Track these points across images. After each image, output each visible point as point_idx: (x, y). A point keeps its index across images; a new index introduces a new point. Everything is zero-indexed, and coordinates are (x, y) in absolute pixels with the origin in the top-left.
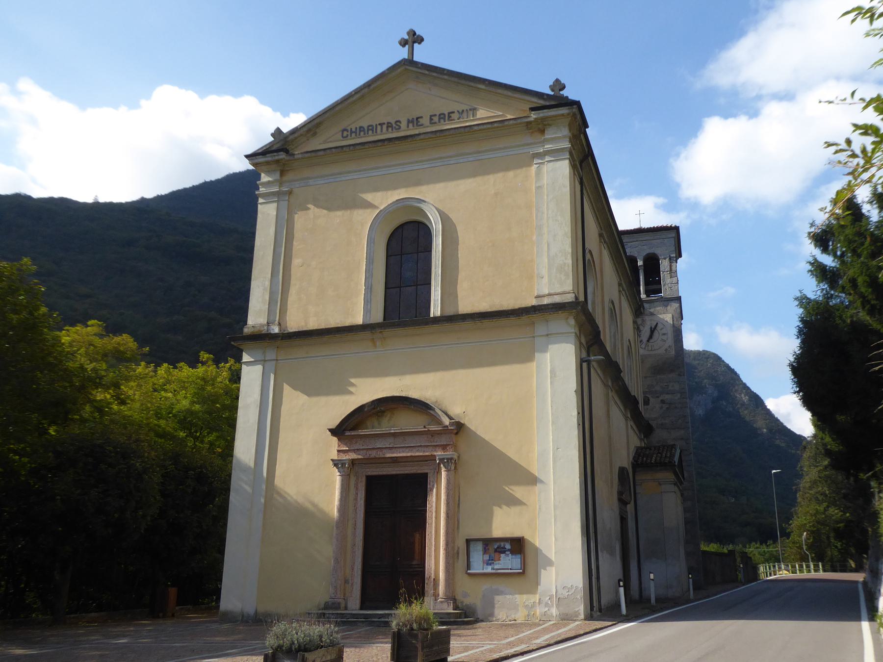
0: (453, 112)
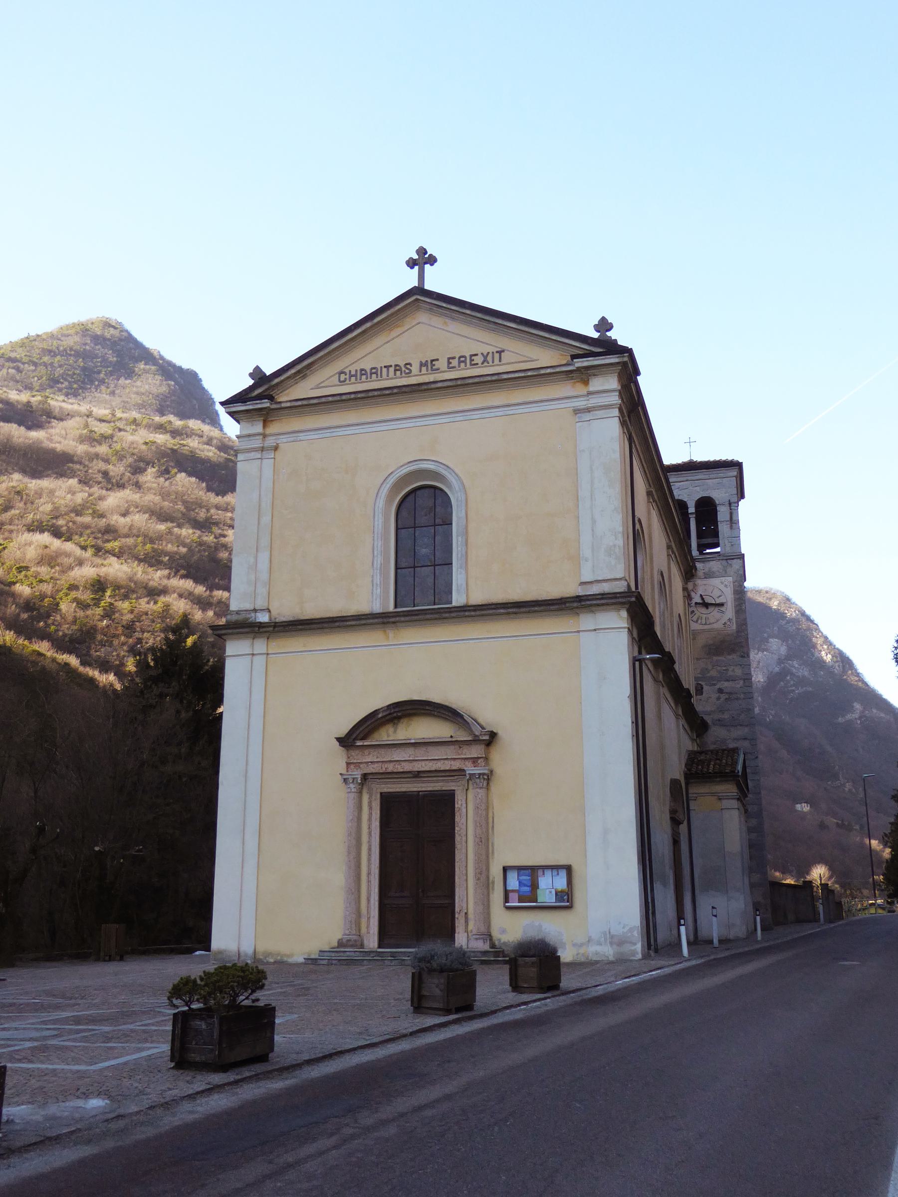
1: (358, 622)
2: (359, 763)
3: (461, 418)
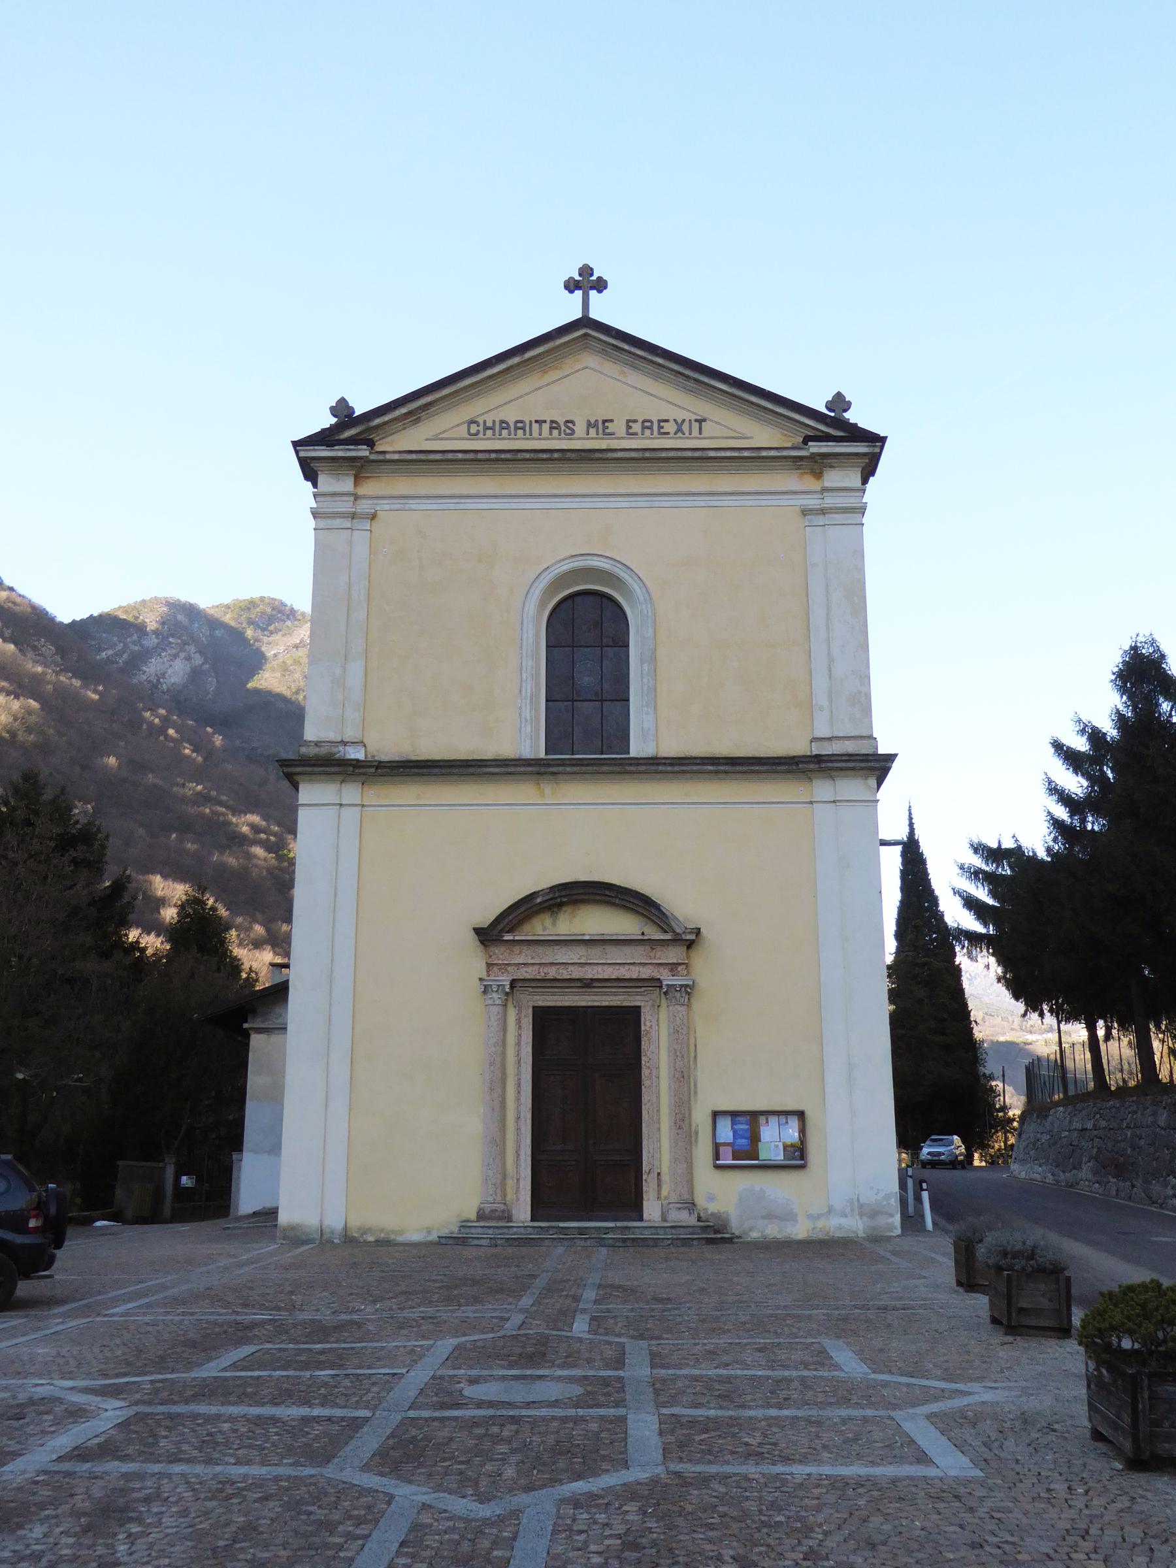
0: (667, 421)
1: (503, 770)
2: (507, 964)
3: (647, 504)
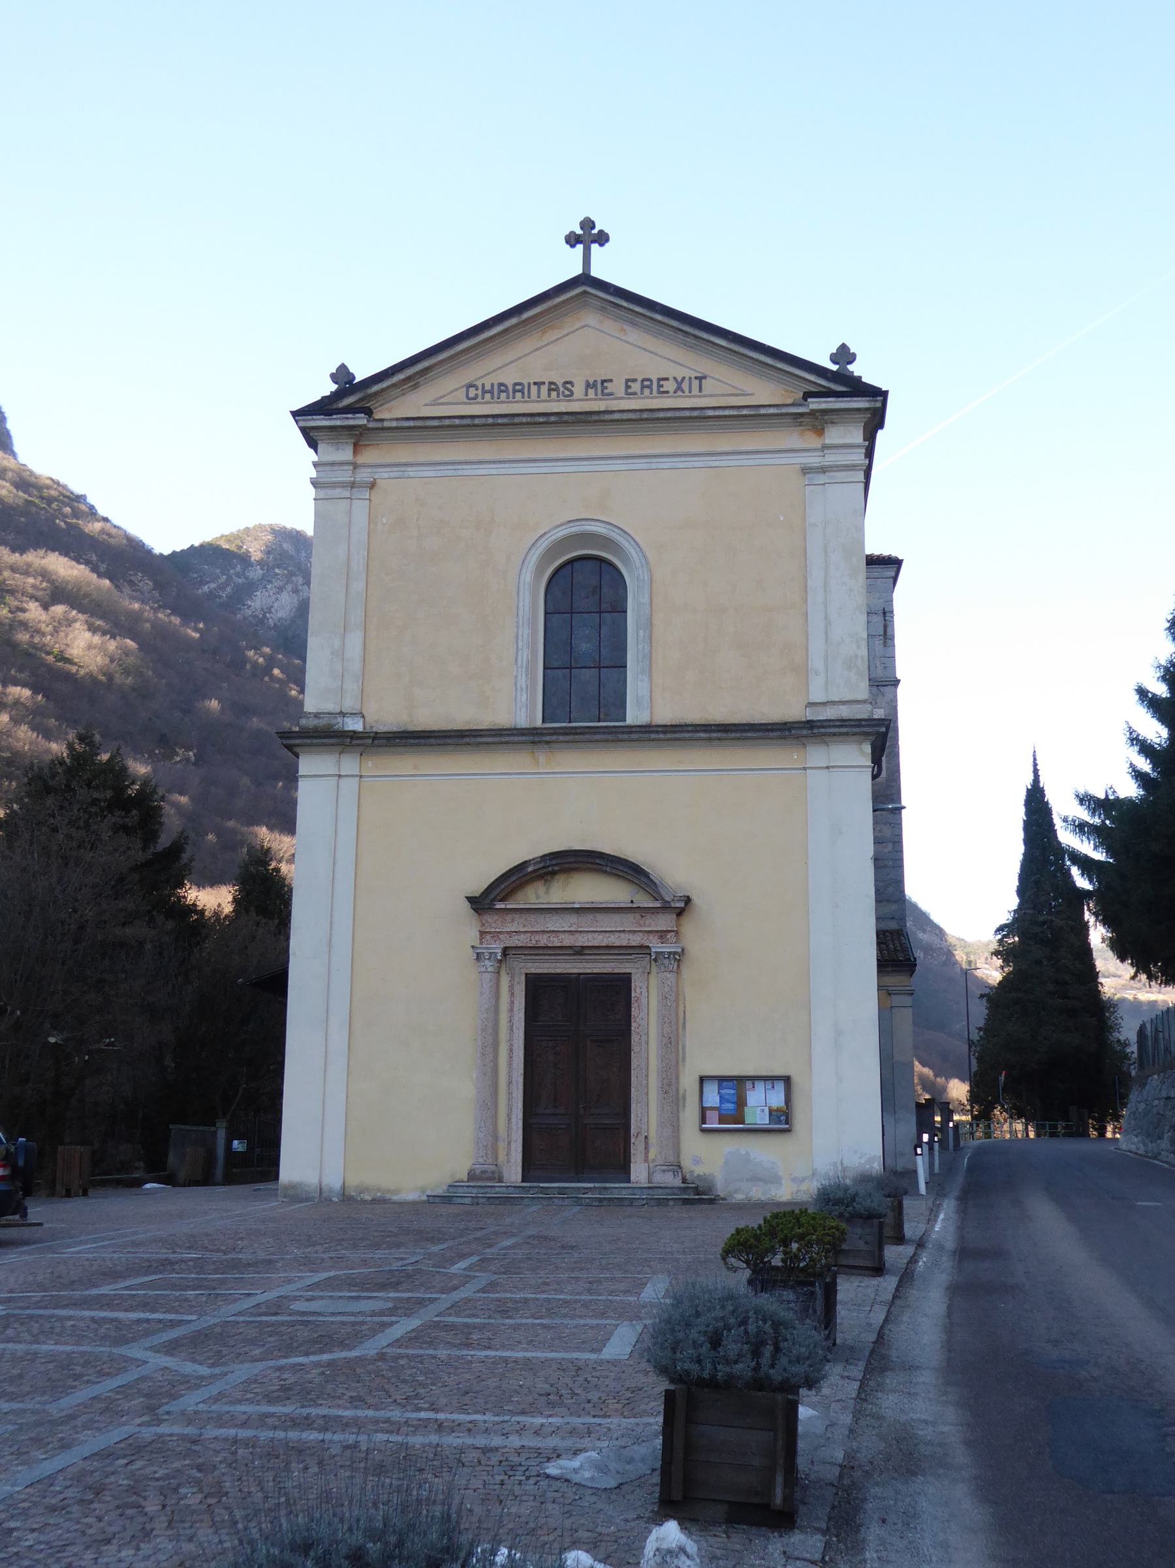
0: (667, 379)
1: (496, 739)
2: (499, 932)
